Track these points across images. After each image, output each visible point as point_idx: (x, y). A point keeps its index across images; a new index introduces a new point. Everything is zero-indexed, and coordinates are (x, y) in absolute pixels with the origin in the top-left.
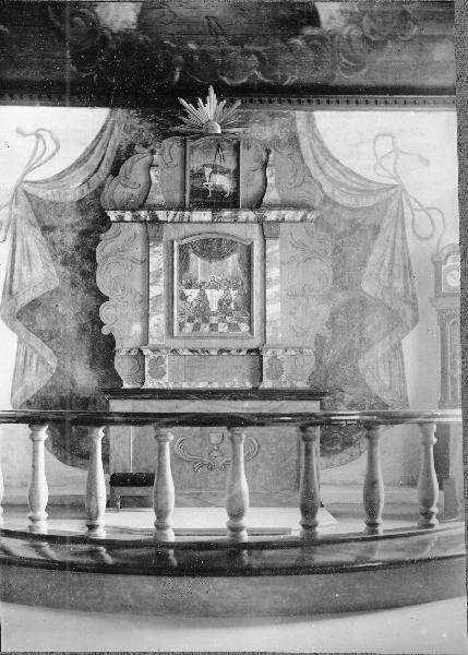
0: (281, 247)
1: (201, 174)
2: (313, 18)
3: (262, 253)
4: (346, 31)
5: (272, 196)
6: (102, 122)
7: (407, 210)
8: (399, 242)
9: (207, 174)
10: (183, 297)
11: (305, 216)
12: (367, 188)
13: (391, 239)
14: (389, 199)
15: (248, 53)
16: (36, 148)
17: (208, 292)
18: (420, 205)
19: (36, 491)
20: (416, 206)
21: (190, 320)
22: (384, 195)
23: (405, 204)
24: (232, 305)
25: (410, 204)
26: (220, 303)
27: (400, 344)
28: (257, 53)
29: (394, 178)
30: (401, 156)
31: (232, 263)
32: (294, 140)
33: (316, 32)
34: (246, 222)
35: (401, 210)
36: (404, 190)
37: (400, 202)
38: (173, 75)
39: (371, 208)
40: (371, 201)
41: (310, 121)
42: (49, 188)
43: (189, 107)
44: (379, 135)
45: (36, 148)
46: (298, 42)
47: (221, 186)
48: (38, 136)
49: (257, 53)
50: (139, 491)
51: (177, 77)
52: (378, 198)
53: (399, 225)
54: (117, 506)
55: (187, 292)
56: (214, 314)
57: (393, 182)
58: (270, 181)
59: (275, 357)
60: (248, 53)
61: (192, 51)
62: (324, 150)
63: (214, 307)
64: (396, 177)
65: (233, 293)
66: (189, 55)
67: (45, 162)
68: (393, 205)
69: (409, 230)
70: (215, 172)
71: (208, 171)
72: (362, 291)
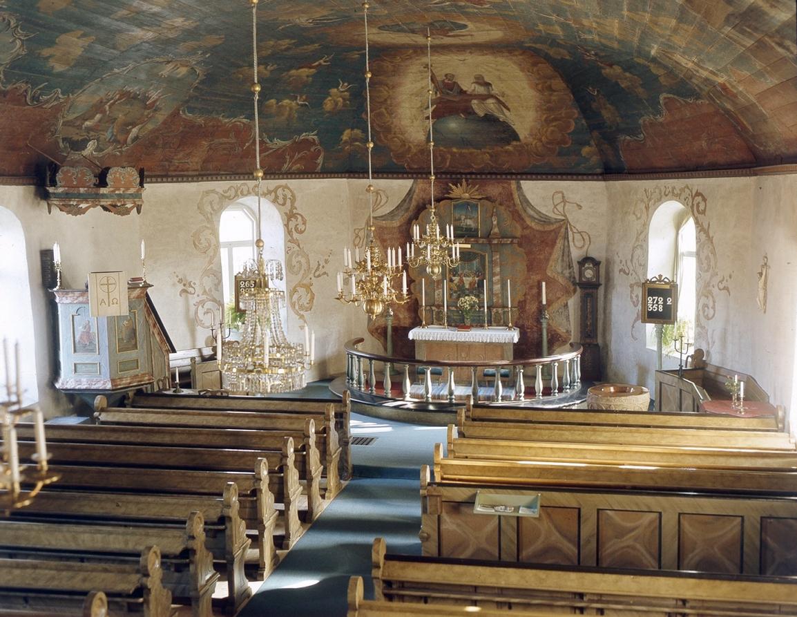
0: (500, 256)
1: (460, 219)
2: (515, 136)
3: (543, 172)
4: (534, 143)
5: (496, 230)
6: (412, 183)
7: (570, 233)
8: (566, 250)
9: (463, 219)
10: (451, 281)
11: (512, 241)
12: (545, 221)
13: (562, 247)
14: (560, 227)
15: (485, 153)
16: (377, 200)
17: (464, 278)
18: (577, 230)
19: (528, 430)
20: (575, 231)
21: (455, 292)
22: (558, 225)
23: (569, 229)
24: (476, 285)
25: (571, 230)
26: (470, 284)
27: (567, 303)
28: (488, 153)
29: (562, 215)
30: (567, 203)
31: (476, 263)
32: (510, 196)
33: (518, 143)
34: (483, 244)
35: (567, 232)
36: (568, 222)
37: (567, 229)
38: (446, 162)
39: (551, 231)
40: (552, 227)
41: (519, 188)
42: (384, 220)
43: (454, 187)
44: (556, 192)
45: (377, 200)
46: (509, 148)
47: (470, 225)
48: (377, 193)
49: (488, 153)
50: (82, 597)
51: (448, 164)
52: (555, 226)
53: (566, 241)
54: (256, 501)
55: (454, 278)
56: (468, 289)
57: (563, 218)
58: (495, 223)
59: (497, 312)
60: (485, 153)
61: (455, 153)
62: (527, 201)
63: (467, 286)
64: (565, 216)
65: (477, 279)
66: (453, 154)
67: (382, 206)
68: (563, 230)
69: (571, 244)
70: (466, 218)
71: (463, 217)
72: (546, 274)
